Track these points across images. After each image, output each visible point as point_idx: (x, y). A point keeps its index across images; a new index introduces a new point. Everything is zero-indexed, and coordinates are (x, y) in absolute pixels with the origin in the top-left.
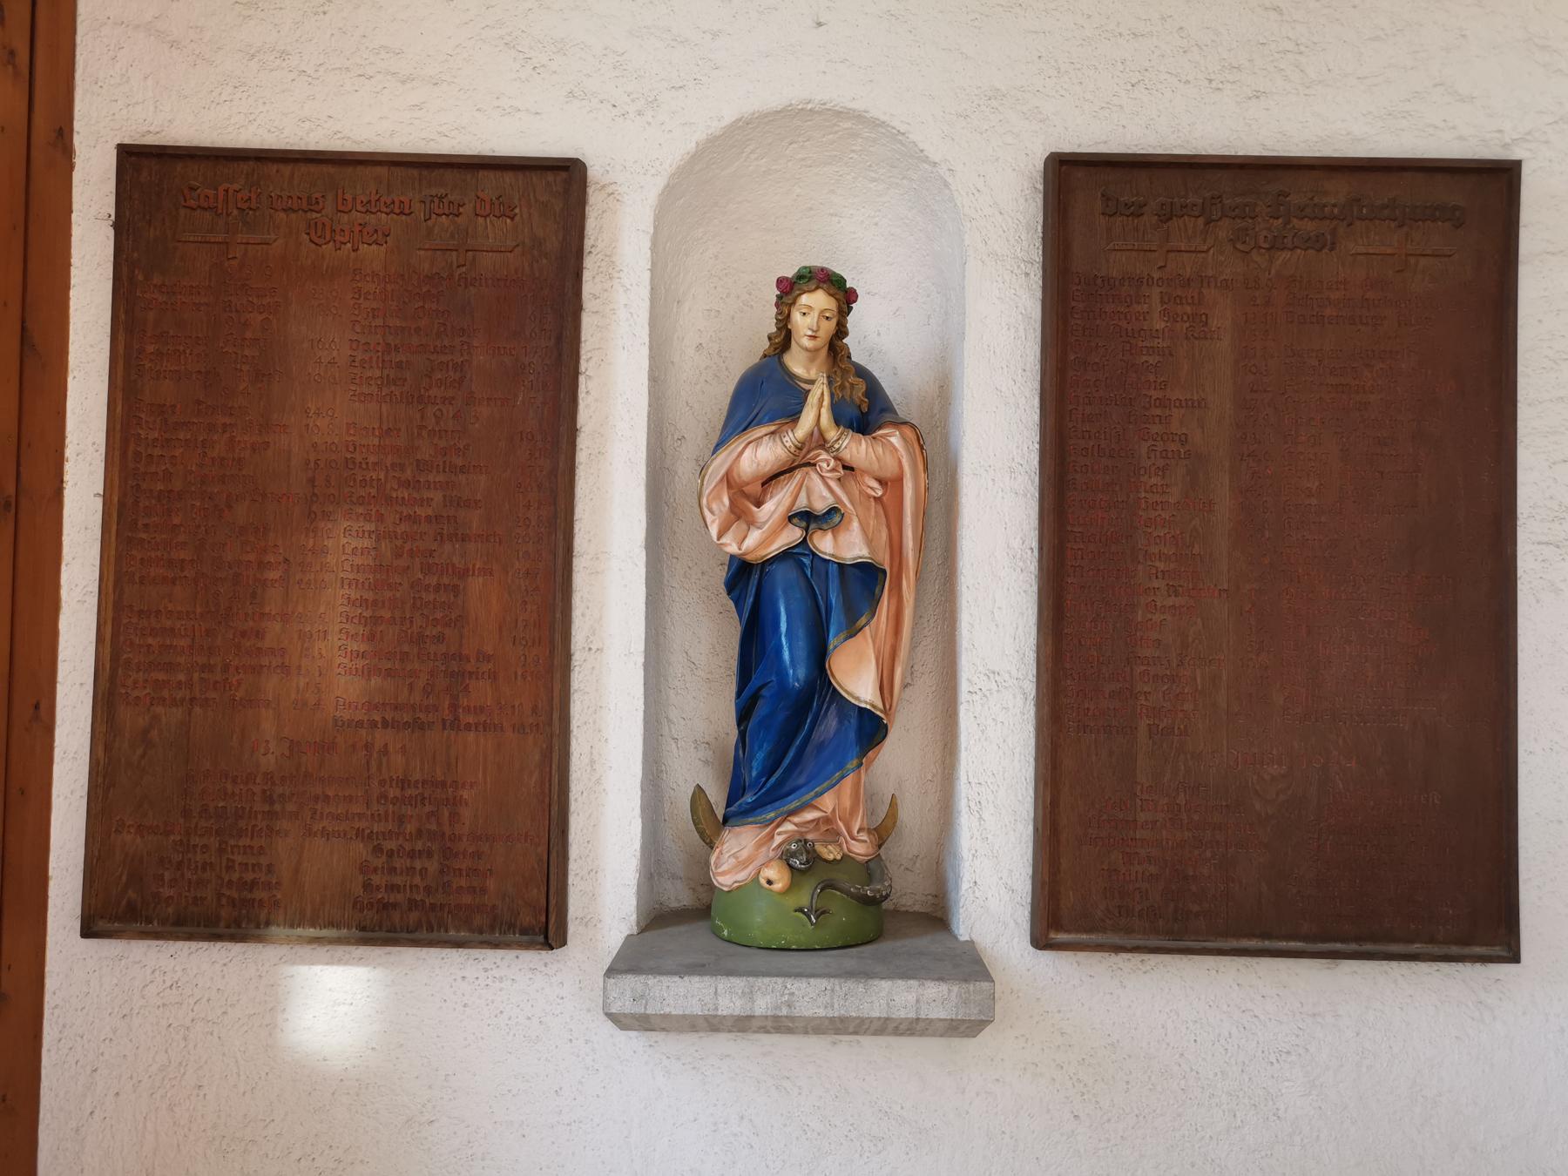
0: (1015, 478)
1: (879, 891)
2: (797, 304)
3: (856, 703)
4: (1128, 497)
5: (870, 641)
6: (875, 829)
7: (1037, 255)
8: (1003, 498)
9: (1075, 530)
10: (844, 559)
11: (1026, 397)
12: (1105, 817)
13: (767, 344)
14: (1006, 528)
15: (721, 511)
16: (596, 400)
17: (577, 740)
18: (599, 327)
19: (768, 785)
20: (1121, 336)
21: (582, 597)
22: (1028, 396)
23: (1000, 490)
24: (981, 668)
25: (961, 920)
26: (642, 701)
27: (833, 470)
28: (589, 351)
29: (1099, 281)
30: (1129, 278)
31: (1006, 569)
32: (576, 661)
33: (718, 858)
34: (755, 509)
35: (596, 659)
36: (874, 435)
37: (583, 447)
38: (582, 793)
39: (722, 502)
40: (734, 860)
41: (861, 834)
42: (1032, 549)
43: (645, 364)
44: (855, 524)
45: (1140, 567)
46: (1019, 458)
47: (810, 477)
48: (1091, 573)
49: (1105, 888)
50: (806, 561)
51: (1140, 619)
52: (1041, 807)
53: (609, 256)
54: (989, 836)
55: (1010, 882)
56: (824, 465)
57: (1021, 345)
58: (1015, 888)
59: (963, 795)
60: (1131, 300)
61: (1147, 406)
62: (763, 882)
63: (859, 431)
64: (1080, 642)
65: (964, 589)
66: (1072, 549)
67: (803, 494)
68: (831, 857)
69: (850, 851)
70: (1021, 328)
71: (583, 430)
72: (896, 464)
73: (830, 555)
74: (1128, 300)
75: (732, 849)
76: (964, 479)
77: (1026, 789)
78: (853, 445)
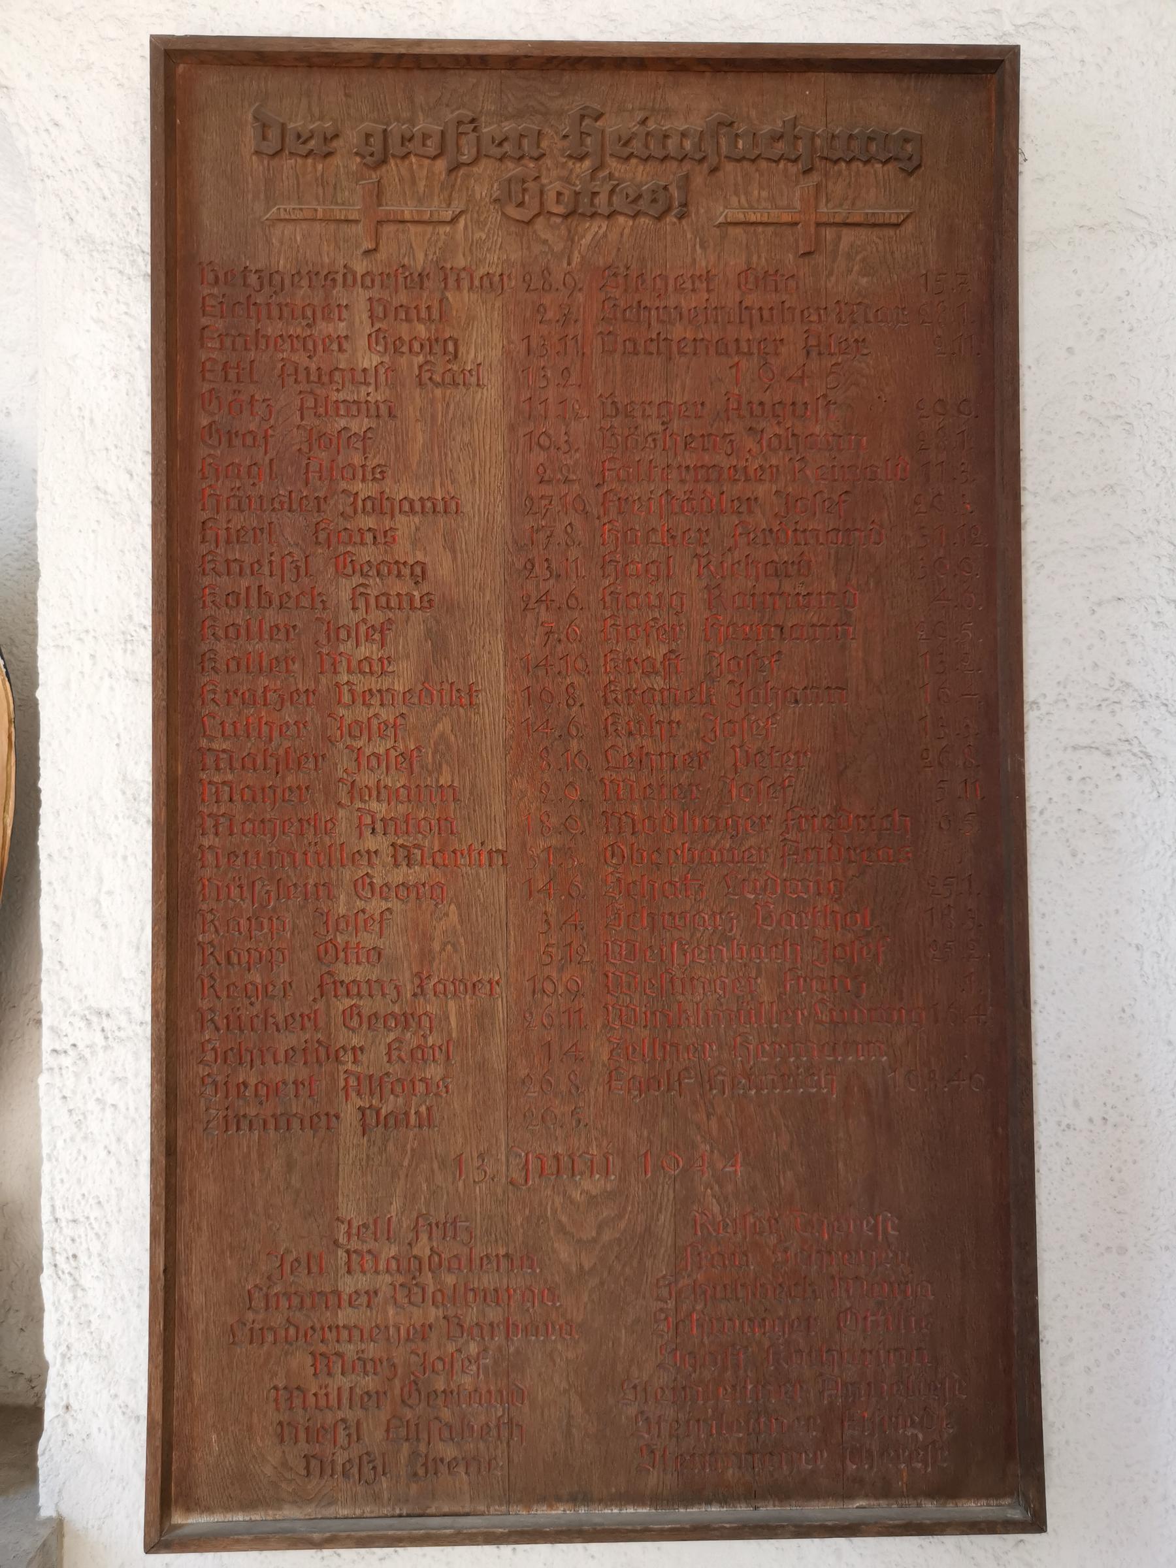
4: (317, 681)
9: (215, 746)
12: (277, 1289)
14: (118, 745)
24: (75, 1006)
29: (253, 279)
54: (92, 1318)
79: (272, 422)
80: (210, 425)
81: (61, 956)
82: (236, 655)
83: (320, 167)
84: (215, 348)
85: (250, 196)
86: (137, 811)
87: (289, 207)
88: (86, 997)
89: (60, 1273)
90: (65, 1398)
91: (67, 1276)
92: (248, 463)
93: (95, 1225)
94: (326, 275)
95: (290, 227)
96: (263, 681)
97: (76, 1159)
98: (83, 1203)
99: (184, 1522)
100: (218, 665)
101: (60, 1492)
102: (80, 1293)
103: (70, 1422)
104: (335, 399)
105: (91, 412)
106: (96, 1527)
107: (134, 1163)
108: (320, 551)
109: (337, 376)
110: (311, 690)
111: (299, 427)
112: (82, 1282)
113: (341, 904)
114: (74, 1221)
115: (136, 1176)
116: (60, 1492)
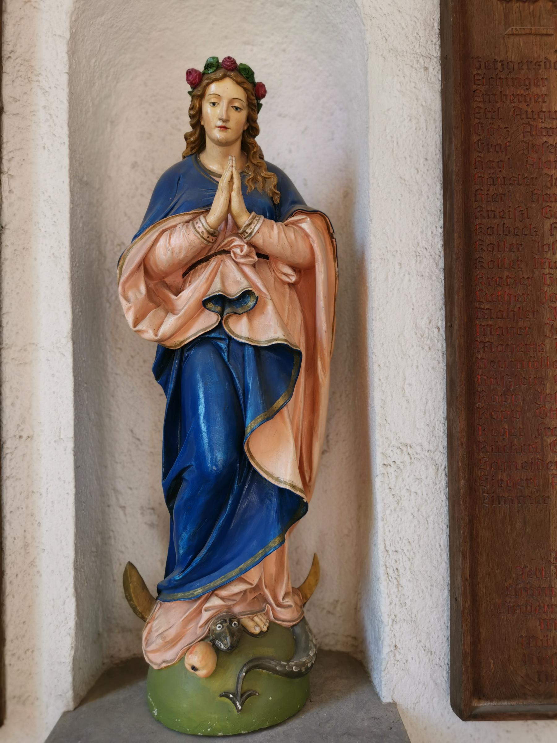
0: (420, 262)
1: (304, 664)
2: (207, 95)
3: (276, 484)
4: (533, 273)
5: (287, 420)
6: (299, 589)
7: (435, 51)
8: (410, 280)
9: (482, 306)
10: (259, 342)
11: (428, 185)
12: (521, 586)
13: (184, 145)
14: (413, 309)
15: (137, 299)
16: (19, 198)
17: (10, 525)
18: (19, 128)
19: (194, 564)
20: (521, 118)
21: (11, 387)
22: (430, 184)
23: (407, 273)
24: (394, 442)
25: (383, 683)
26: (72, 484)
27: (247, 256)
28: (11, 152)
29: (499, 65)
30: (527, 62)
31: (415, 347)
32: (7, 448)
33: (149, 633)
34: (173, 297)
35: (27, 446)
36: (286, 222)
37: (8, 244)
38: (17, 575)
39: (139, 291)
40: (161, 641)
41: (286, 600)
42: (438, 328)
43: (66, 162)
44: (270, 308)
45: (547, 341)
46: (424, 242)
47: (225, 264)
48: (500, 348)
49: (524, 655)
50: (223, 345)
51: (548, 391)
52: (459, 578)
53: (28, 61)
54: (407, 601)
55: (428, 645)
56: (238, 251)
57: (423, 135)
58: (433, 650)
59: (381, 562)
60: (530, 84)
61: (549, 184)
62: (189, 668)
63: (271, 218)
64: (491, 415)
65: (376, 368)
66: (481, 325)
67: (218, 280)
68: (257, 631)
69: (276, 618)
70: (422, 120)
71: (7, 227)
72: (308, 250)
73: (245, 338)
74: (527, 83)
75: (160, 628)
76: (373, 265)
77: (441, 555)
78: (265, 230)
79: (509, 139)
80: (478, 141)
81: (386, 417)
82: (492, 259)
83: (532, 7)
84: (480, 102)
85: (497, 22)
86: (423, 343)
87: (518, 28)
88: (399, 438)
89: (390, 578)
90: (394, 642)
91: (394, 579)
92: (497, 160)
93: (408, 554)
94: (536, 63)
95: (517, 39)
96: (506, 273)
97: (397, 520)
98: (400, 542)
99: (478, 705)
100: (484, 265)
101: (394, 690)
102: (400, 588)
103: (397, 654)
104: (540, 127)
105: (397, 138)
106: (412, 708)
107: (426, 522)
108: (534, 205)
109: (542, 115)
110: (530, 277)
111: (522, 141)
112: (401, 583)
113: (548, 388)
114: (396, 551)
115: (427, 528)
116: (394, 690)
